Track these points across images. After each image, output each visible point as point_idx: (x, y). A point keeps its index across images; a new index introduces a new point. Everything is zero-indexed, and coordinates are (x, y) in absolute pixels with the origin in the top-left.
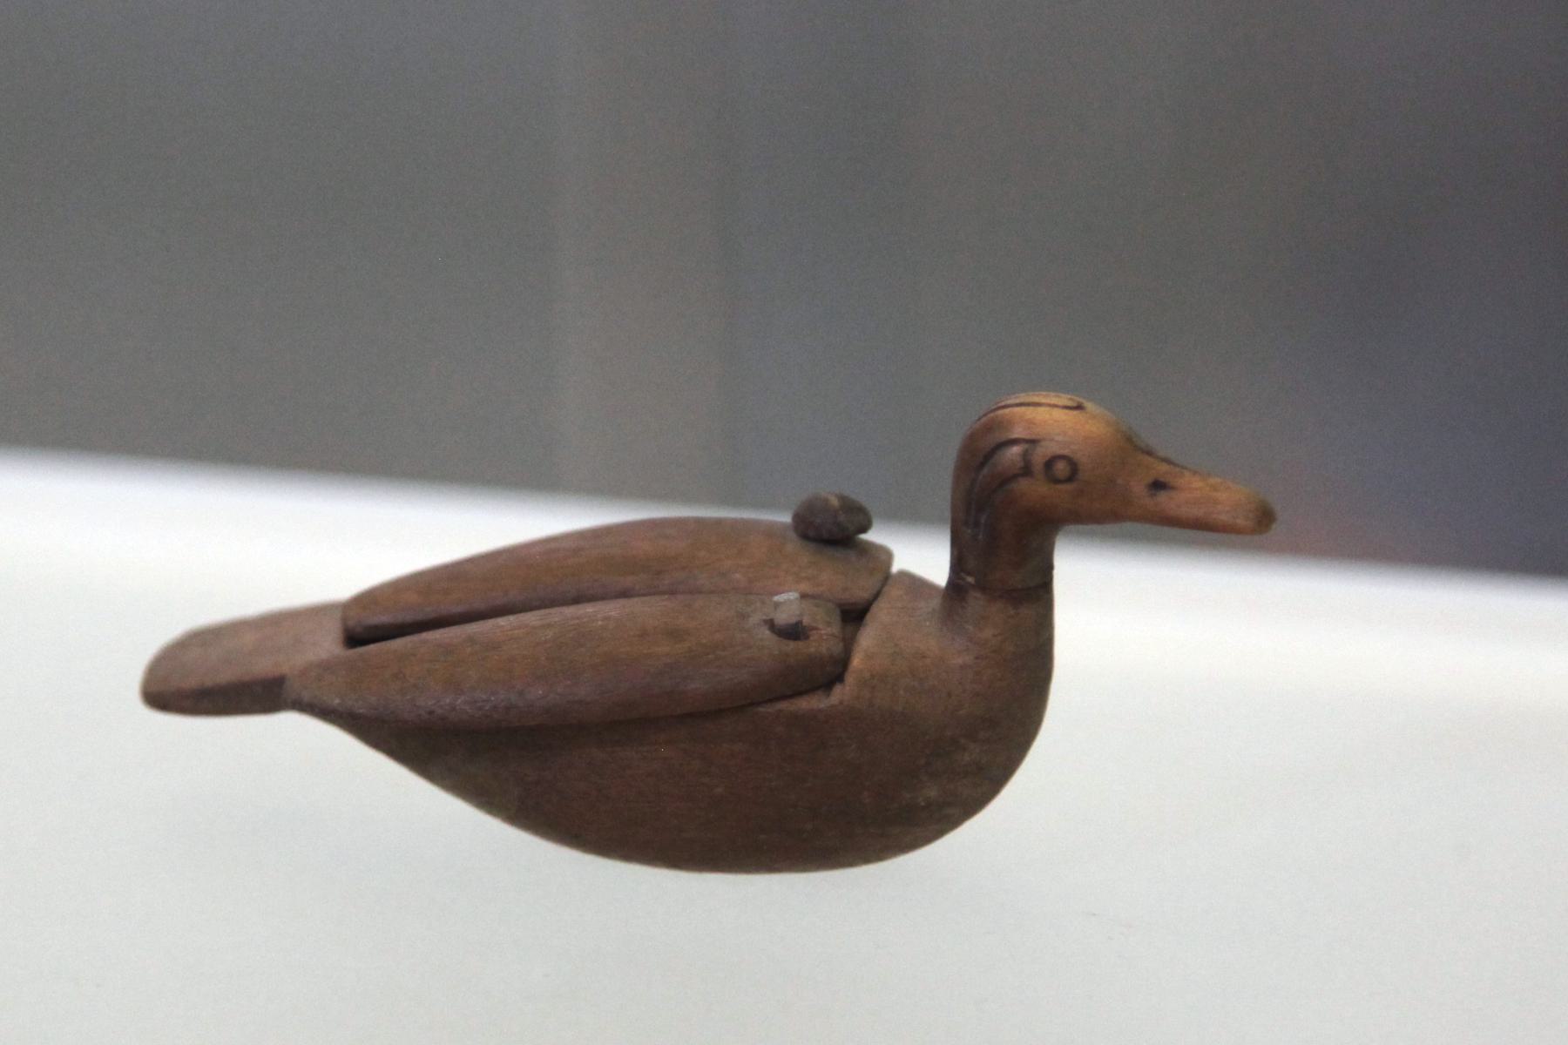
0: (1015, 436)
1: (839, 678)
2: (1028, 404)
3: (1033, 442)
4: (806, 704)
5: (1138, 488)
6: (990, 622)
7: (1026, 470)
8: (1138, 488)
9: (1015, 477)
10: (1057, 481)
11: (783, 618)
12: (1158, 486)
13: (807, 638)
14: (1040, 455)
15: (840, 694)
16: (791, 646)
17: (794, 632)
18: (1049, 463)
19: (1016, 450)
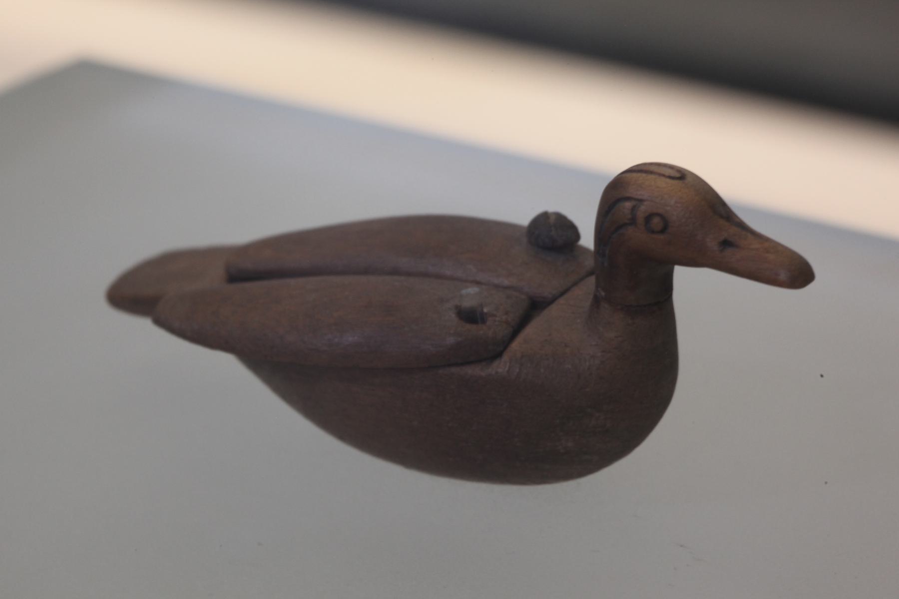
0: (628, 195)
1: (499, 355)
2: (426, 275)
3: (641, 201)
4: (470, 371)
5: (712, 244)
6: (783, 276)
7: (633, 221)
8: (712, 244)
9: (625, 225)
10: (653, 232)
11: (467, 304)
12: (726, 244)
13: (484, 321)
14: (643, 210)
15: (500, 367)
16: (472, 328)
17: (470, 316)
18: (648, 218)
19: (628, 205)
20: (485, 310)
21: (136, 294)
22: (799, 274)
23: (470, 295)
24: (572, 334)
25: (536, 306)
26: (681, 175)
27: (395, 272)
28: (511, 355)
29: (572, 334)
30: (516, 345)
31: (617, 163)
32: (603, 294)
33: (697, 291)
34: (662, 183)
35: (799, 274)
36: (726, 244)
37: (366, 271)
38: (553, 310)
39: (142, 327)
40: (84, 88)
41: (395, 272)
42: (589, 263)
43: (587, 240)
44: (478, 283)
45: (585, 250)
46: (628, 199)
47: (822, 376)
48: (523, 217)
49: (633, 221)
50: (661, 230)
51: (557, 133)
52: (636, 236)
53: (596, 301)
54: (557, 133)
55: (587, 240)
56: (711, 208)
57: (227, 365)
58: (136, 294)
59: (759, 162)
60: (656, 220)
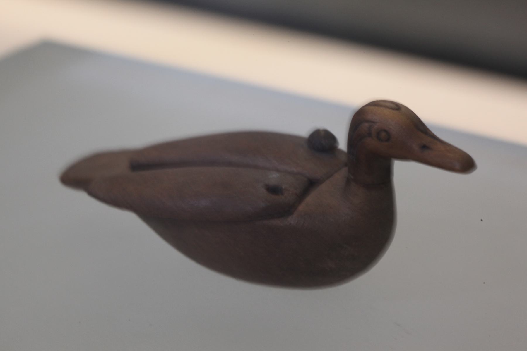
3: (374, 122)
6: (458, 166)
12: (424, 147)
15: (292, 220)
17: (274, 190)
19: (367, 125)
20: (283, 187)
21: (77, 177)
22: (465, 164)
23: (274, 178)
24: (333, 200)
25: (312, 184)
26: (397, 107)
27: (230, 164)
28: (298, 212)
29: (333, 200)
30: (301, 207)
31: (359, 98)
32: (352, 177)
33: (408, 177)
34: (387, 112)
35: (465, 164)
36: (424, 147)
37: (212, 163)
38: (324, 187)
39: (81, 197)
40: (46, 56)
41: (230, 164)
42: (344, 158)
43: (342, 144)
44: (278, 171)
45: (341, 152)
46: (367, 121)
47: (482, 220)
48: (302, 129)
49: (370, 135)
50: (386, 139)
51: (324, 84)
52: (372, 143)
53: (348, 182)
54: (324, 84)
55: (342, 144)
56: (415, 125)
57: (130, 220)
58: (77, 177)
59: (445, 101)
60: (383, 134)
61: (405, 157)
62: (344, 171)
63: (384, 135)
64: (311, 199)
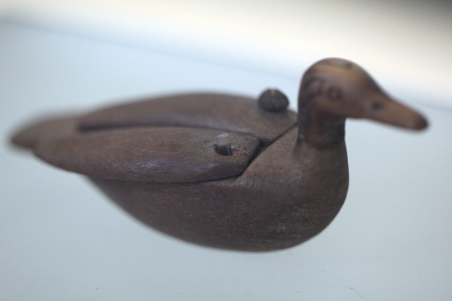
15: (241, 182)
17: (223, 151)
21: (59, 142)
22: (419, 123)
23: (223, 138)
24: (284, 162)
25: (263, 145)
26: (348, 65)
27: (178, 125)
29: (284, 162)
33: (359, 134)
35: (419, 123)
38: (274, 147)
42: (295, 119)
43: (294, 105)
44: (227, 131)
45: (292, 112)
48: (253, 89)
52: (322, 102)
53: (299, 142)
55: (294, 105)
56: (368, 85)
57: (76, 186)
61: (359, 115)
62: (295, 131)
63: (335, 94)
64: (259, 159)
